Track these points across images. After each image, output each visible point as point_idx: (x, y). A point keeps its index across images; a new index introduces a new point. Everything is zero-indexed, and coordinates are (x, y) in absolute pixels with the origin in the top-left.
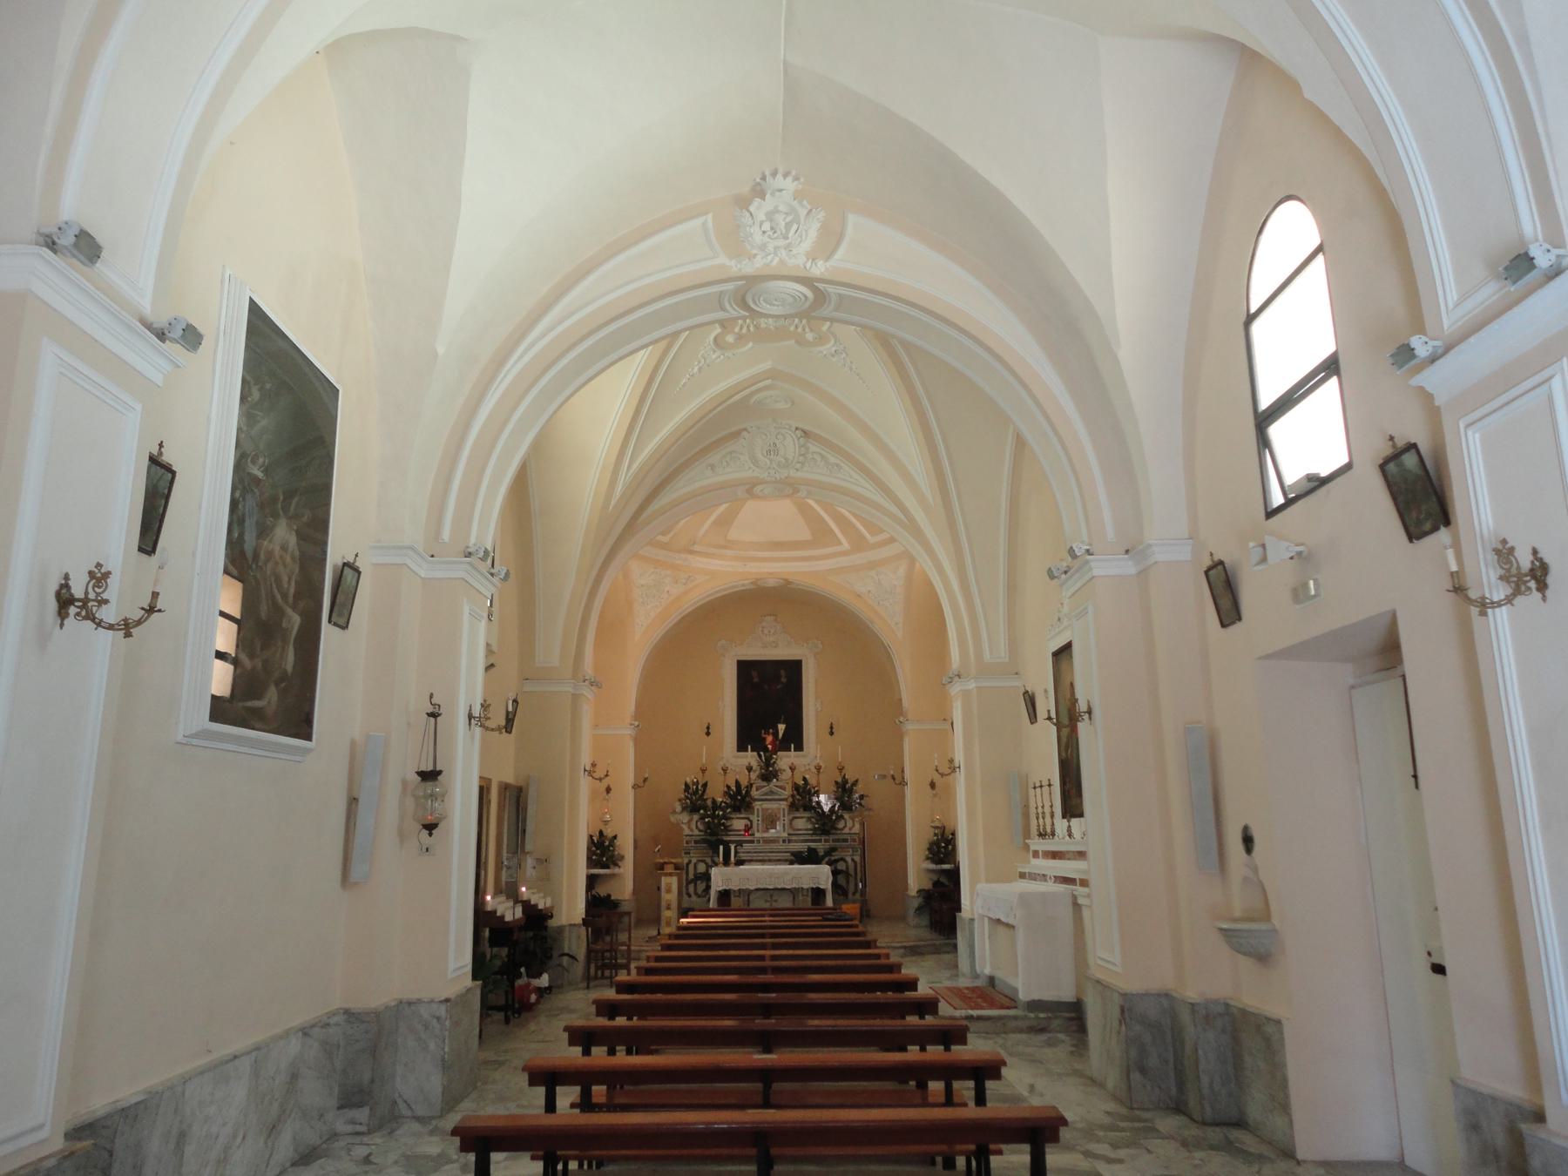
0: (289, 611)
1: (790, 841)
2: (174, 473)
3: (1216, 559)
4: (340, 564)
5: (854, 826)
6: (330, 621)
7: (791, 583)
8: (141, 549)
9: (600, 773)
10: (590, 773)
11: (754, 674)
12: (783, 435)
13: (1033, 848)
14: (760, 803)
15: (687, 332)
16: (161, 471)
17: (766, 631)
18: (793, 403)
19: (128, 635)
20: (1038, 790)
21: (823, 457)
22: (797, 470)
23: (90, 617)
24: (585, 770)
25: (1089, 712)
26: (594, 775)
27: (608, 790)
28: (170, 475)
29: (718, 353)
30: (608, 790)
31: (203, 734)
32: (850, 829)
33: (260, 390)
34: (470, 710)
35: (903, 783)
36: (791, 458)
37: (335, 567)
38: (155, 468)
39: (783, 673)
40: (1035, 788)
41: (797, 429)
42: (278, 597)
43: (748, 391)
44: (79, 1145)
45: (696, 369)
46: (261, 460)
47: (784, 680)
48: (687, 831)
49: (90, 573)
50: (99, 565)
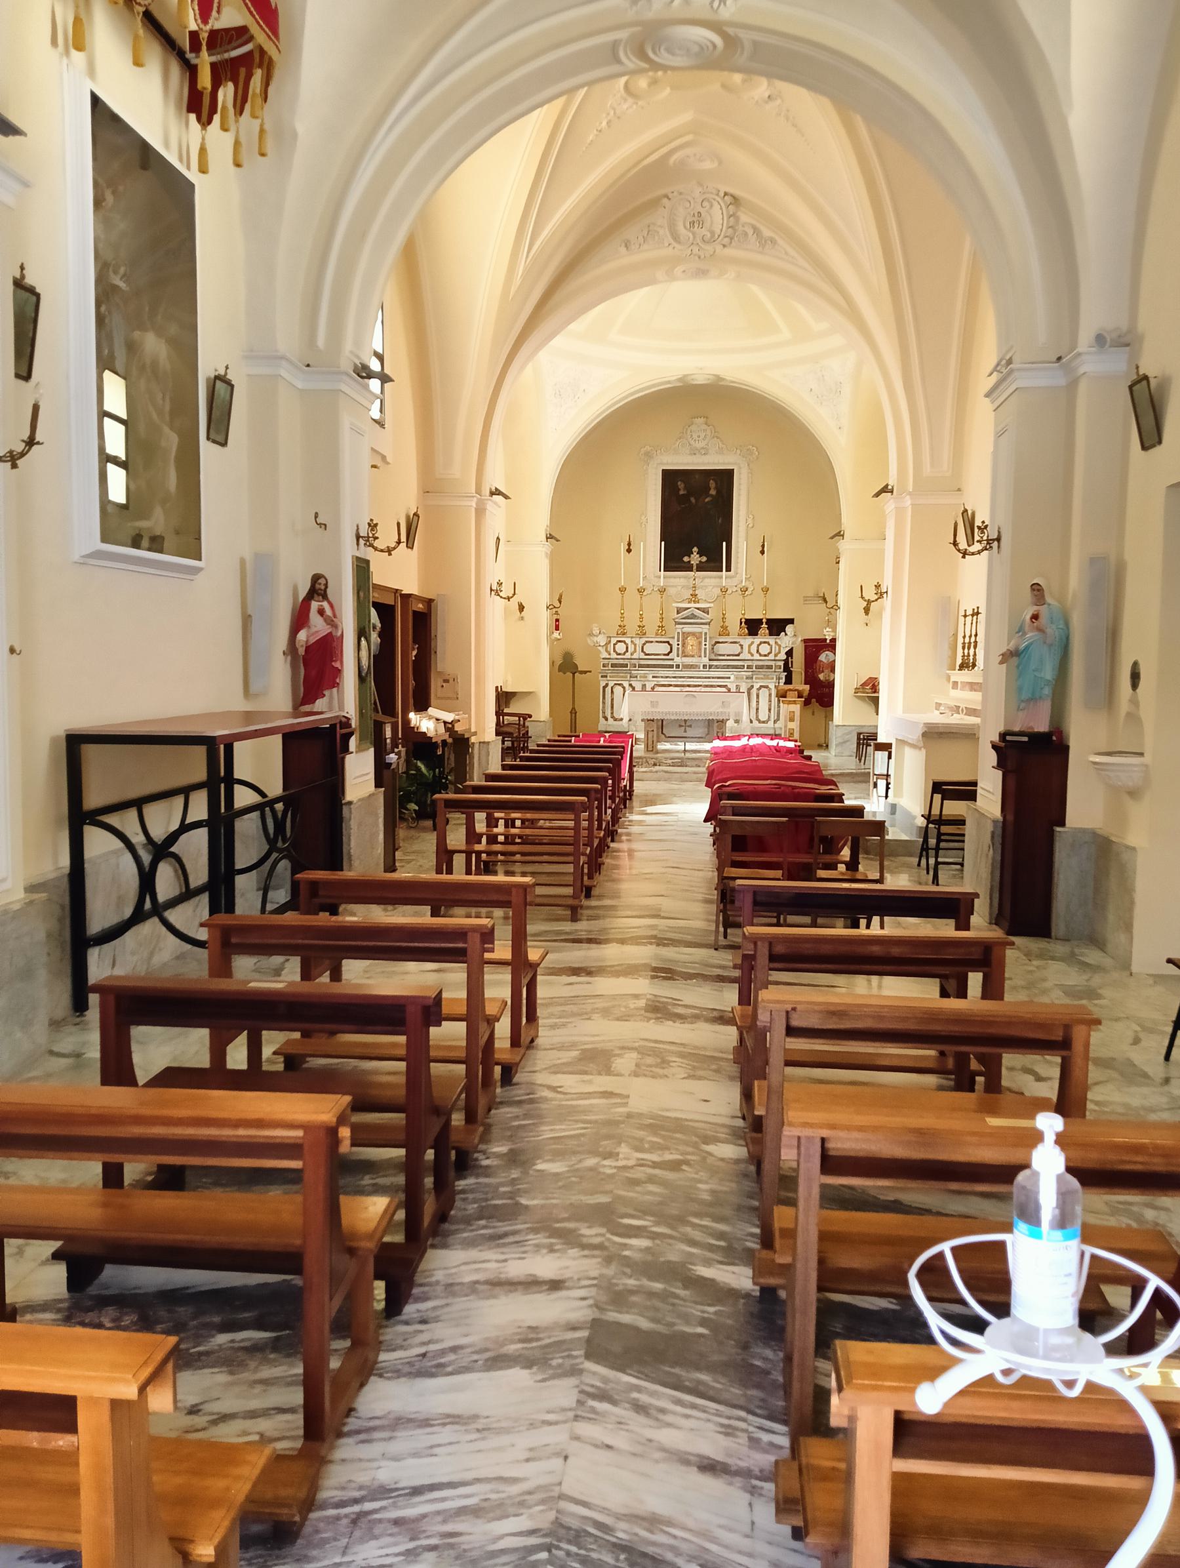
0: (166, 430)
1: (710, 667)
2: (38, 296)
3: (1141, 373)
4: (213, 376)
5: (635, 651)
6: (208, 438)
7: (723, 379)
8: (18, 376)
9: (506, 591)
11: (681, 485)
12: (708, 201)
13: (953, 679)
14: (681, 626)
15: (586, 89)
16: (27, 295)
17: (695, 436)
18: (720, 163)
20: (969, 619)
21: (756, 230)
22: (724, 246)
23: (371, 545)
24: (491, 590)
26: (501, 594)
27: (521, 608)
28: (34, 298)
29: (630, 100)
30: (521, 608)
31: (97, 555)
32: (776, 656)
33: (114, 193)
35: (836, 607)
36: (718, 231)
37: (208, 380)
38: (20, 291)
39: (712, 484)
40: (965, 616)
41: (726, 194)
42: (155, 416)
43: (664, 150)
44: (36, 896)
45: (604, 124)
46: (122, 270)
47: (713, 492)
48: (605, 655)
50: (372, 520)
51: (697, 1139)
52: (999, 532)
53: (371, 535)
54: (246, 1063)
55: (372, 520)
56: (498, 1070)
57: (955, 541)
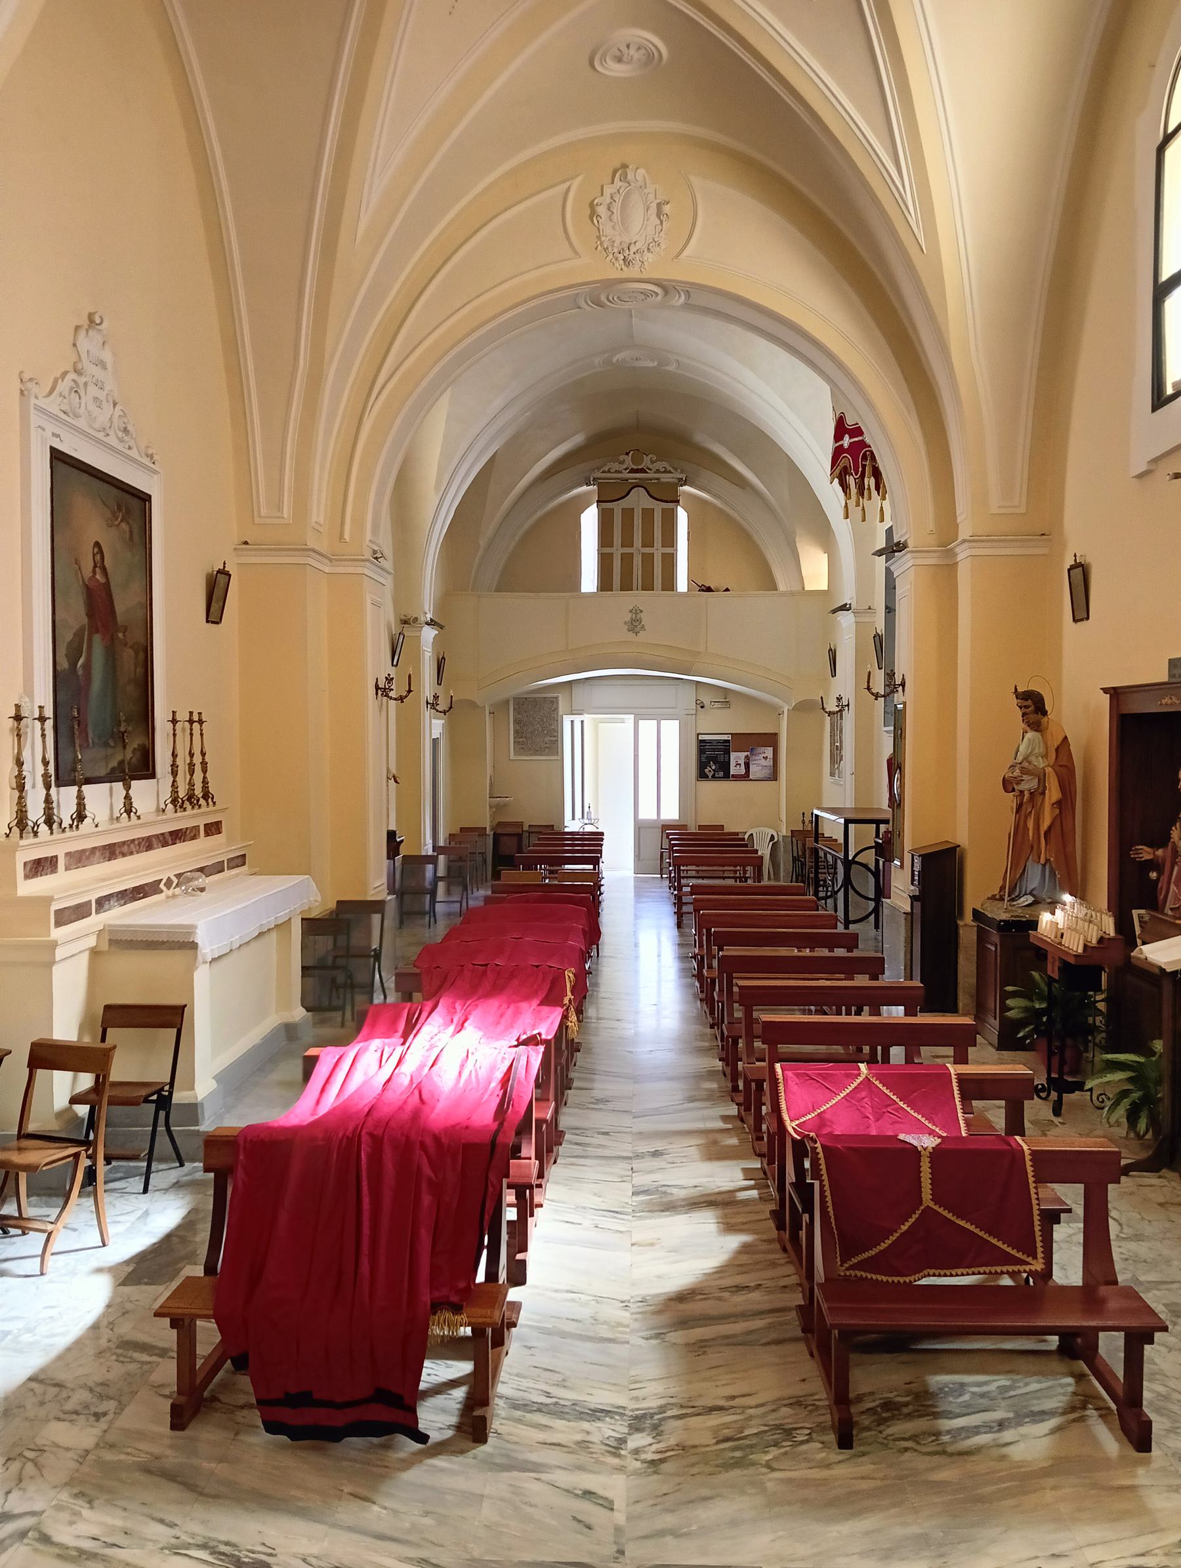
10: (433, 706)
19: (402, 702)
23: (387, 695)
24: (427, 703)
25: (903, 685)
26: (437, 708)
34: (377, 682)
49: (386, 678)
50: (389, 675)
51: (200, 1216)
52: (903, 678)
53: (387, 687)
54: (1081, 1280)
55: (389, 675)
56: (753, 1085)
57: (868, 686)
